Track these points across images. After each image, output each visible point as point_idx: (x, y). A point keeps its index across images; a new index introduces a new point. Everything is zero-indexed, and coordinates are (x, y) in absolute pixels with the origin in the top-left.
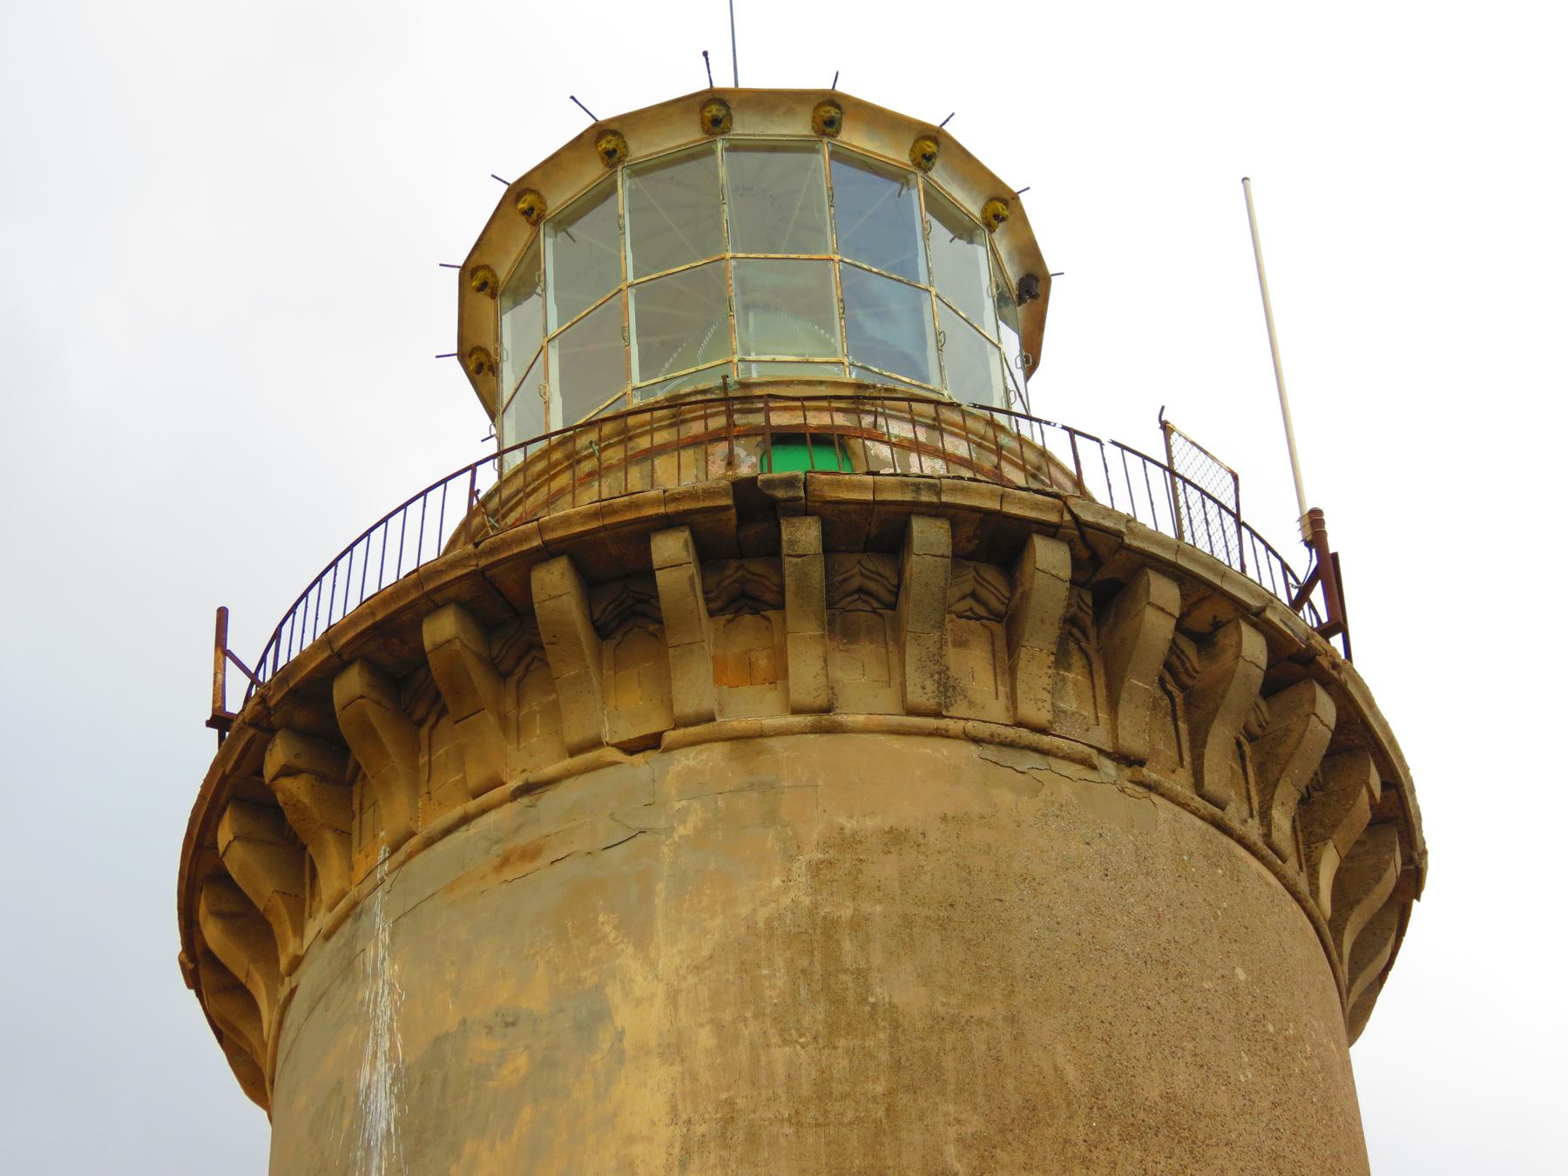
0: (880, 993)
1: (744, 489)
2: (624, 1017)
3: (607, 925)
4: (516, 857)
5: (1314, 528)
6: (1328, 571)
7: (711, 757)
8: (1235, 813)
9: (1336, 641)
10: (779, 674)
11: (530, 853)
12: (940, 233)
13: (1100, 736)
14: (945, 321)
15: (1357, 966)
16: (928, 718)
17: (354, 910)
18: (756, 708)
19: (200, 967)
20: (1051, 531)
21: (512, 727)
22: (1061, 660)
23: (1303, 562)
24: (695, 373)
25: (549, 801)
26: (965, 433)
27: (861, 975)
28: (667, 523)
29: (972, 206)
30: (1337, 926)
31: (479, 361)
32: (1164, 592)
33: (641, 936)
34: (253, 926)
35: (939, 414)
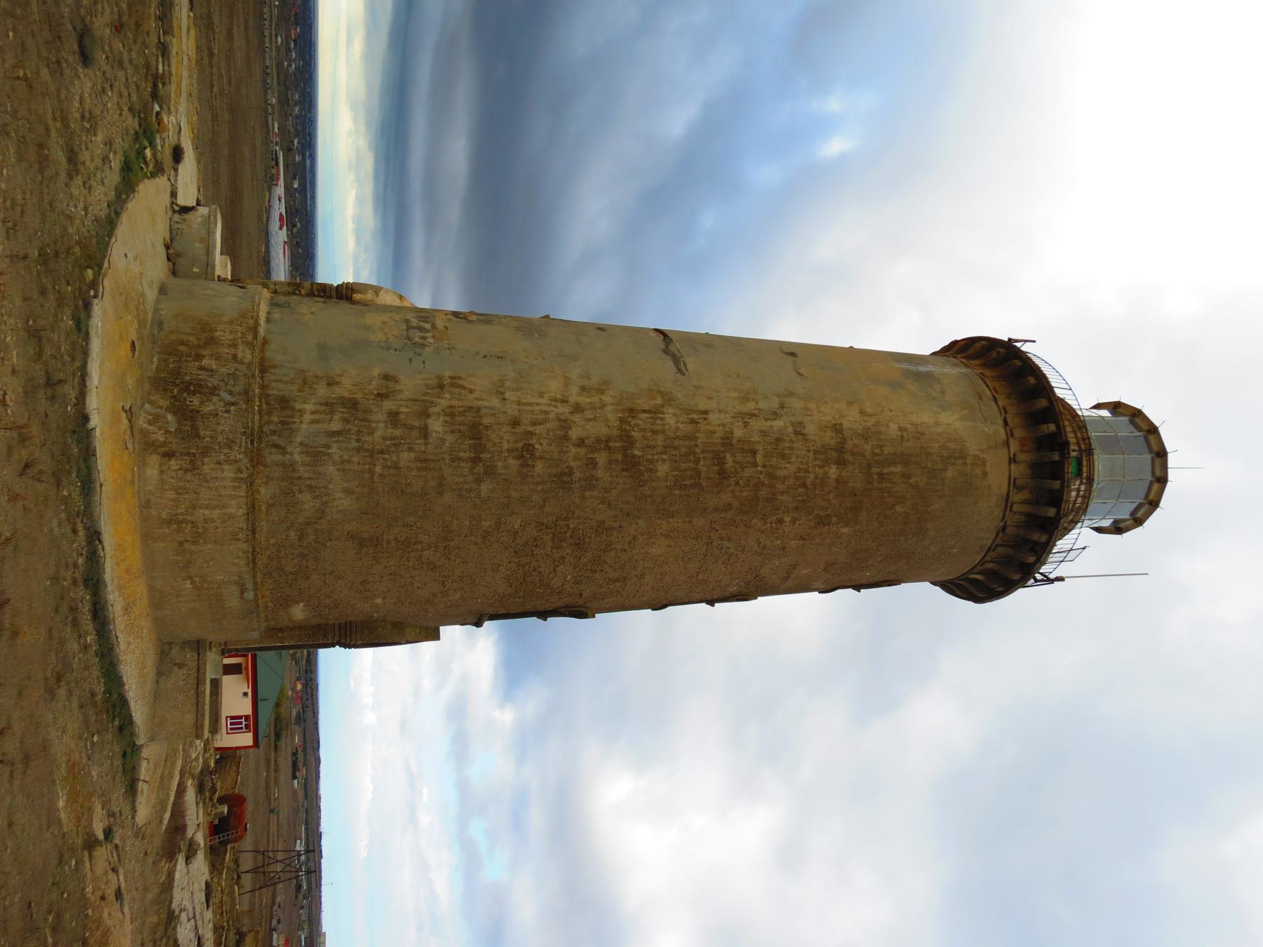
0: (950, 468)
1: (1067, 443)
2: (944, 414)
3: (965, 412)
4: (980, 396)
5: (1060, 579)
6: (1051, 581)
7: (1004, 437)
8: (991, 553)
9: (1032, 581)
10: (1022, 451)
11: (981, 399)
12: (1134, 506)
13: (1009, 523)
14: (1109, 506)
15: (956, 585)
16: (1013, 484)
17: (967, 366)
18: (1014, 447)
19: (954, 343)
20: (1058, 513)
21: (1009, 396)
22: (1028, 515)
23: (1052, 576)
24: (1095, 445)
25: (993, 403)
26: (1082, 503)
27: (954, 464)
28: (1058, 427)
29: (1139, 514)
30: (964, 580)
31: (1098, 406)
32: (1044, 538)
33: (961, 419)
34: (959, 352)
35: (1087, 497)
